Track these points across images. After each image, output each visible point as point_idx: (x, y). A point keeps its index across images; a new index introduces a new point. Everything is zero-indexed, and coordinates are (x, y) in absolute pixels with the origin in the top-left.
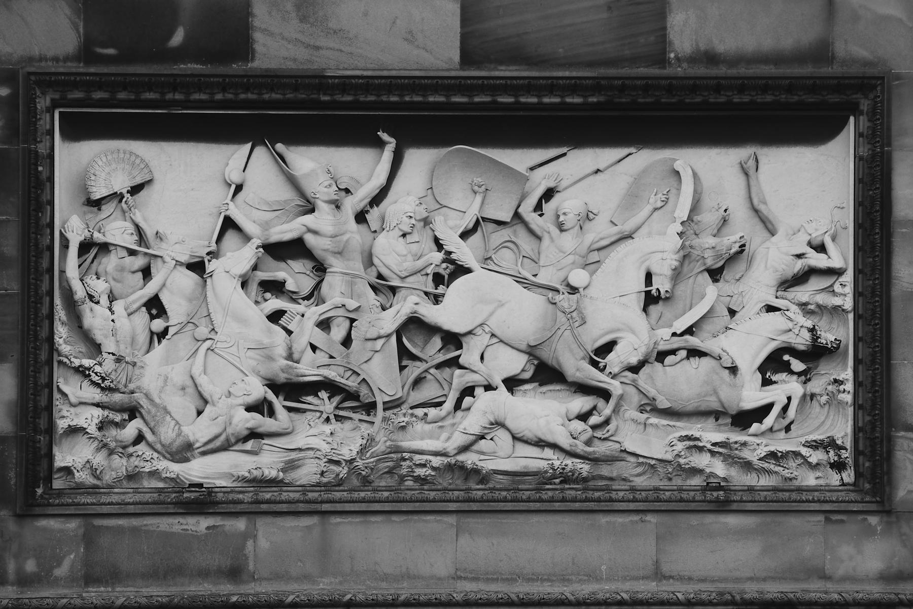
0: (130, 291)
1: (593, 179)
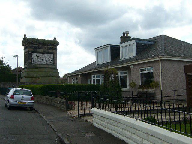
0: (162, 67)
1: (46, 55)
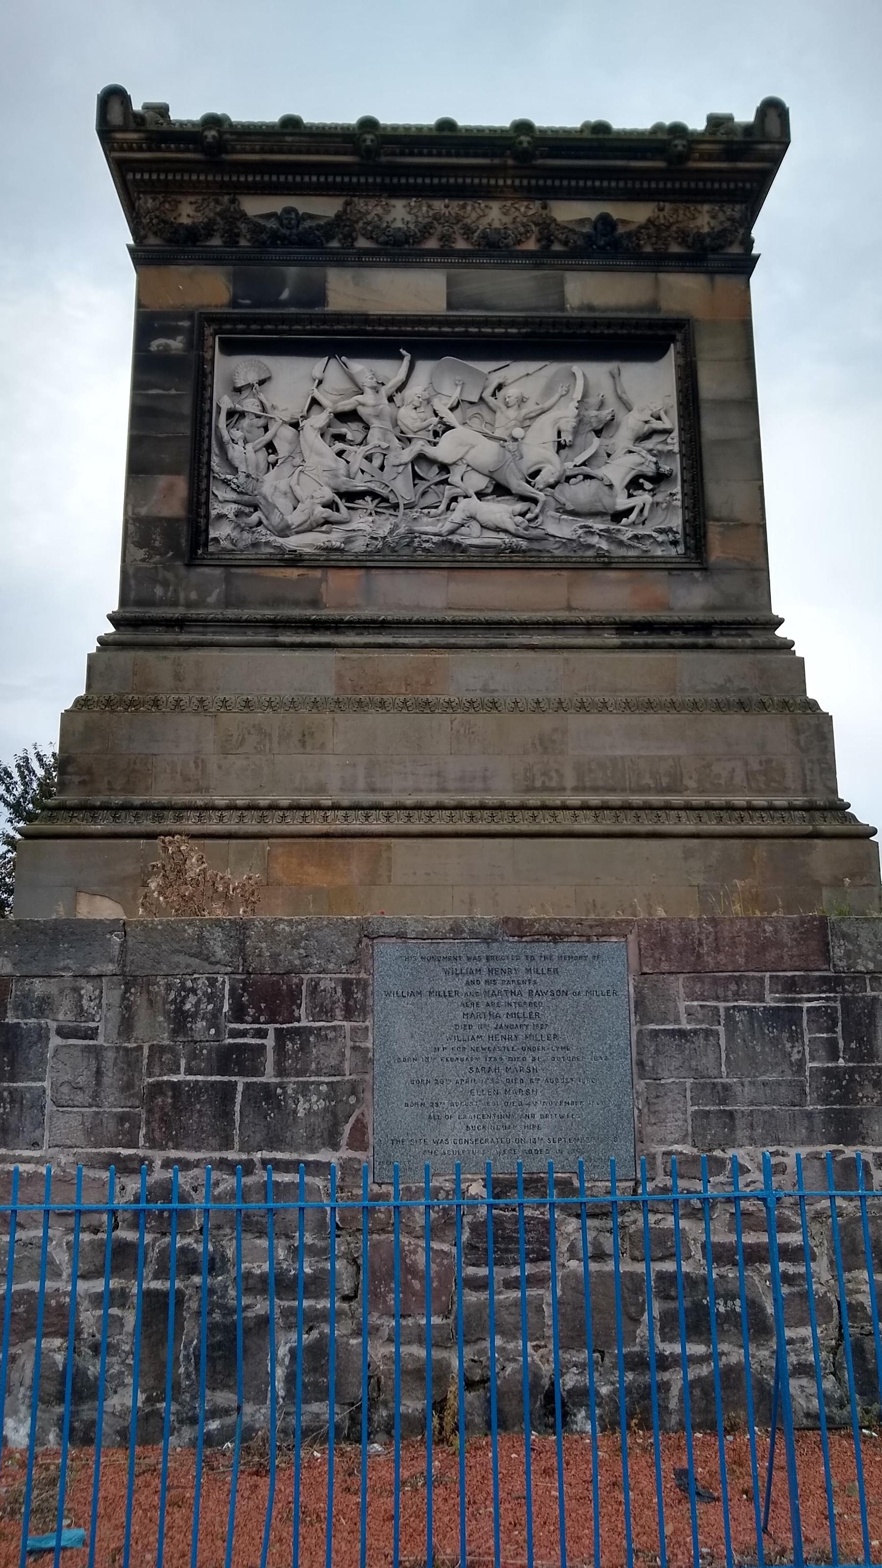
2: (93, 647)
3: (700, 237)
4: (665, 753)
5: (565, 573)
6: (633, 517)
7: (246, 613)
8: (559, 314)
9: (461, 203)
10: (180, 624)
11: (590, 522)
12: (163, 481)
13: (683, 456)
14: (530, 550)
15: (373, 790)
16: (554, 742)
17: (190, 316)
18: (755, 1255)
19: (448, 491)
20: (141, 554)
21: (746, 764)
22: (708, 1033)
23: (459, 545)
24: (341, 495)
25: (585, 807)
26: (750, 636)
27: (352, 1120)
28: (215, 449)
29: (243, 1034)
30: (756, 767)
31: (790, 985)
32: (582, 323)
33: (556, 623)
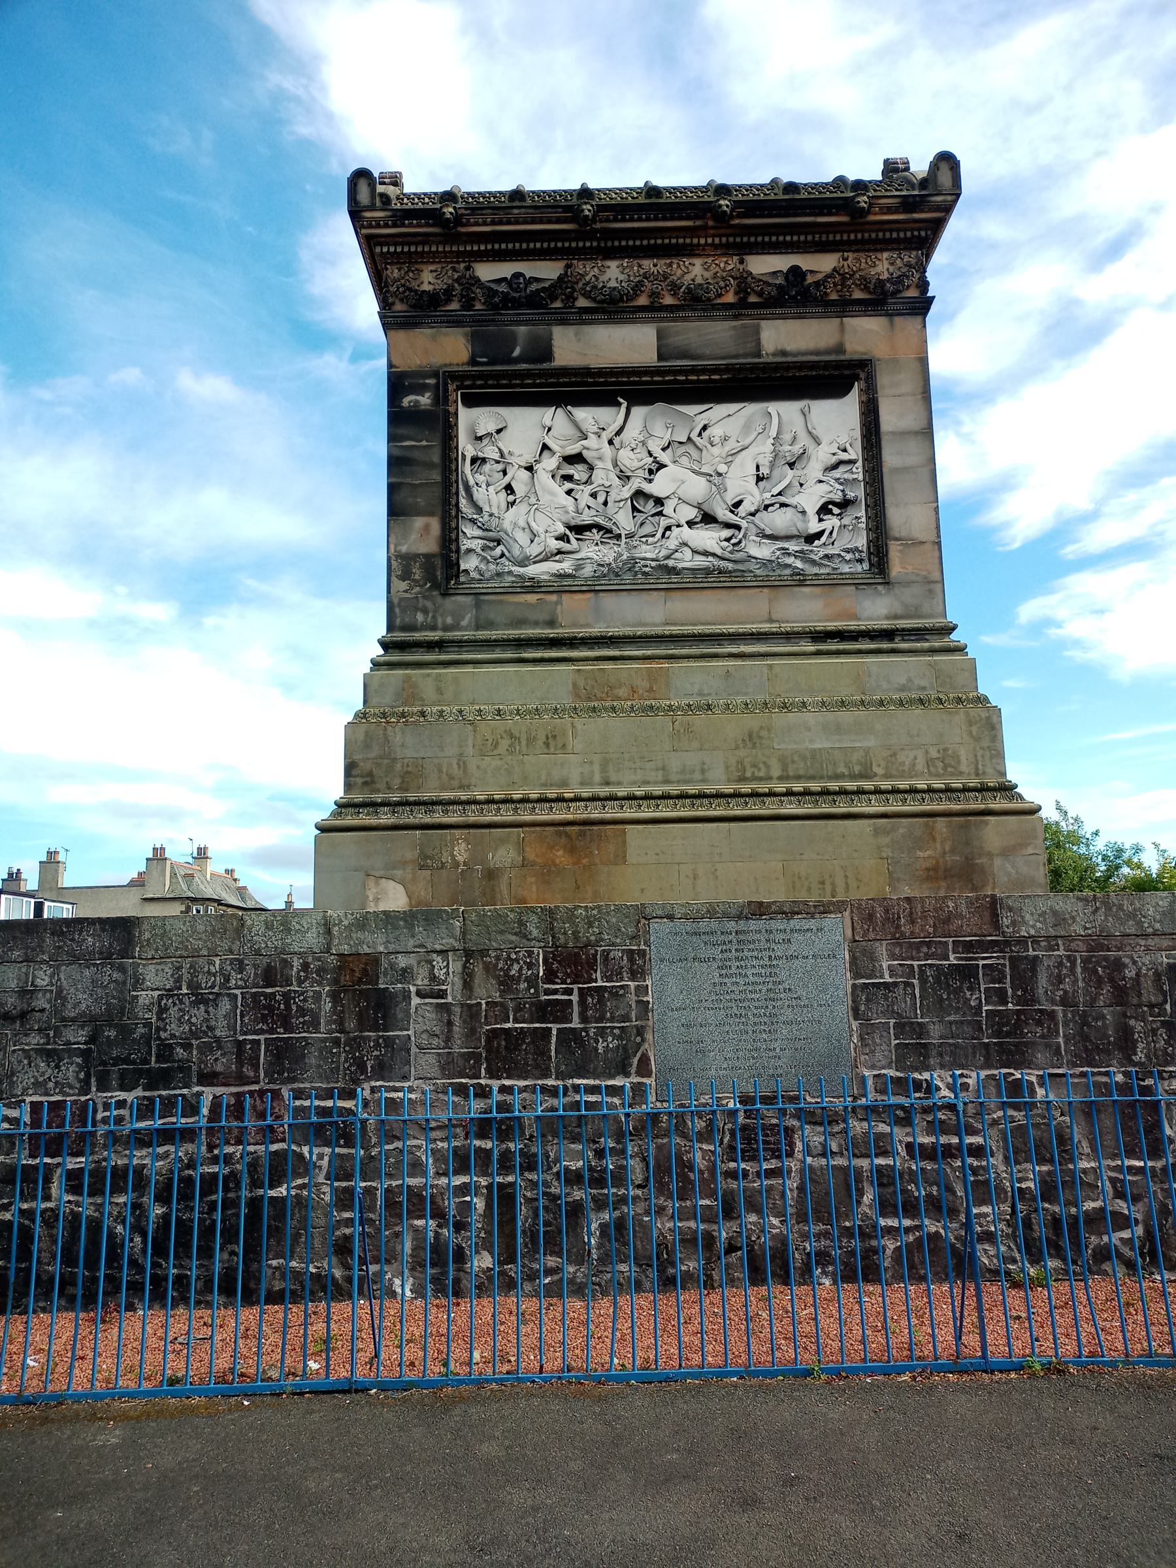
1: (727, 420)
2: (367, 667)
3: (881, 283)
4: (858, 745)
5: (765, 590)
6: (823, 539)
7: (494, 634)
8: (757, 360)
9: (668, 261)
10: (439, 645)
11: (786, 545)
12: (419, 522)
13: (866, 483)
14: (735, 571)
15: (607, 783)
16: (760, 737)
17: (435, 374)
18: (949, 1152)
19: (664, 522)
20: (404, 585)
21: (927, 752)
22: (907, 984)
23: (674, 568)
24: (570, 528)
25: (790, 793)
26: (927, 640)
27: (639, 1055)
28: (462, 492)
29: (555, 992)
30: (934, 754)
31: (969, 947)
32: (777, 367)
33: (760, 634)
